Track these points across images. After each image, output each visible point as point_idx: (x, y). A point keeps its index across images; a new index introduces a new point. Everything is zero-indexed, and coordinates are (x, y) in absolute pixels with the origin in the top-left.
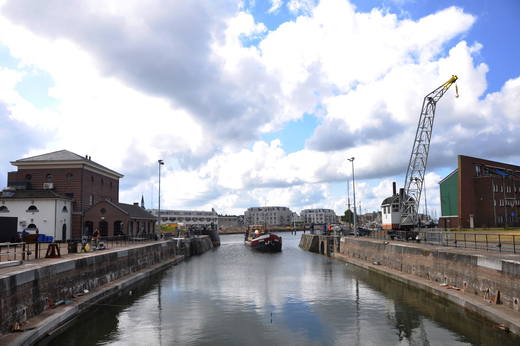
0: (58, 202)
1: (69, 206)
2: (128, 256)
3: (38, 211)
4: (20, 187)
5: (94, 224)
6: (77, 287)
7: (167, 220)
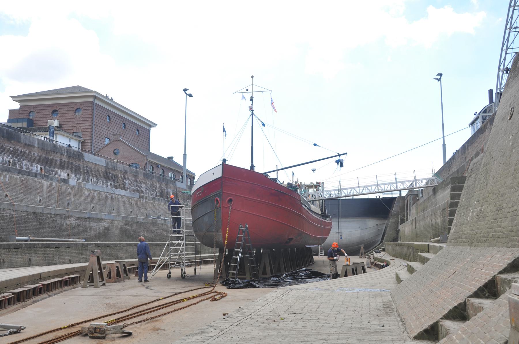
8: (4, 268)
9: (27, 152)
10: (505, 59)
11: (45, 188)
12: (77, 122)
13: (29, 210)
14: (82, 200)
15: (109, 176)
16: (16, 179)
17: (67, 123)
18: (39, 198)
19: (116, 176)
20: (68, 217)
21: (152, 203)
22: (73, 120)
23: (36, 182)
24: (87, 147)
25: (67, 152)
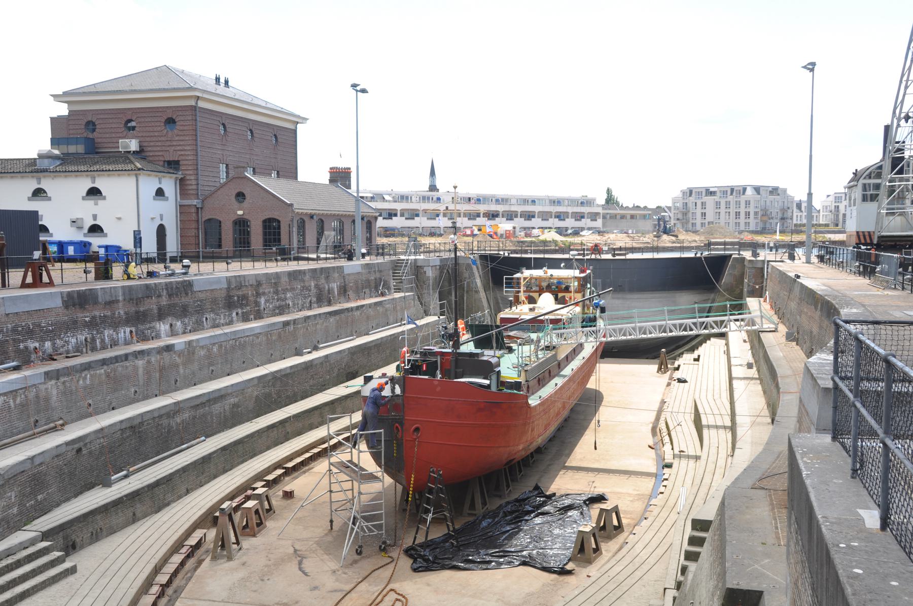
0: (142, 179)
1: (169, 186)
2: (229, 289)
3: (104, 198)
4: (72, 149)
5: (223, 225)
6: (67, 342)
7: (478, 215)
8: (103, 538)
9: (109, 313)
10: (902, 102)
11: (141, 371)
12: (168, 143)
13: (123, 427)
14: (195, 366)
15: (234, 302)
16: (100, 375)
17: (152, 144)
18: (133, 390)
19: (245, 297)
20: (178, 411)
21: (304, 327)
22: (163, 139)
23: (127, 367)
24: (190, 187)
25: (167, 289)
